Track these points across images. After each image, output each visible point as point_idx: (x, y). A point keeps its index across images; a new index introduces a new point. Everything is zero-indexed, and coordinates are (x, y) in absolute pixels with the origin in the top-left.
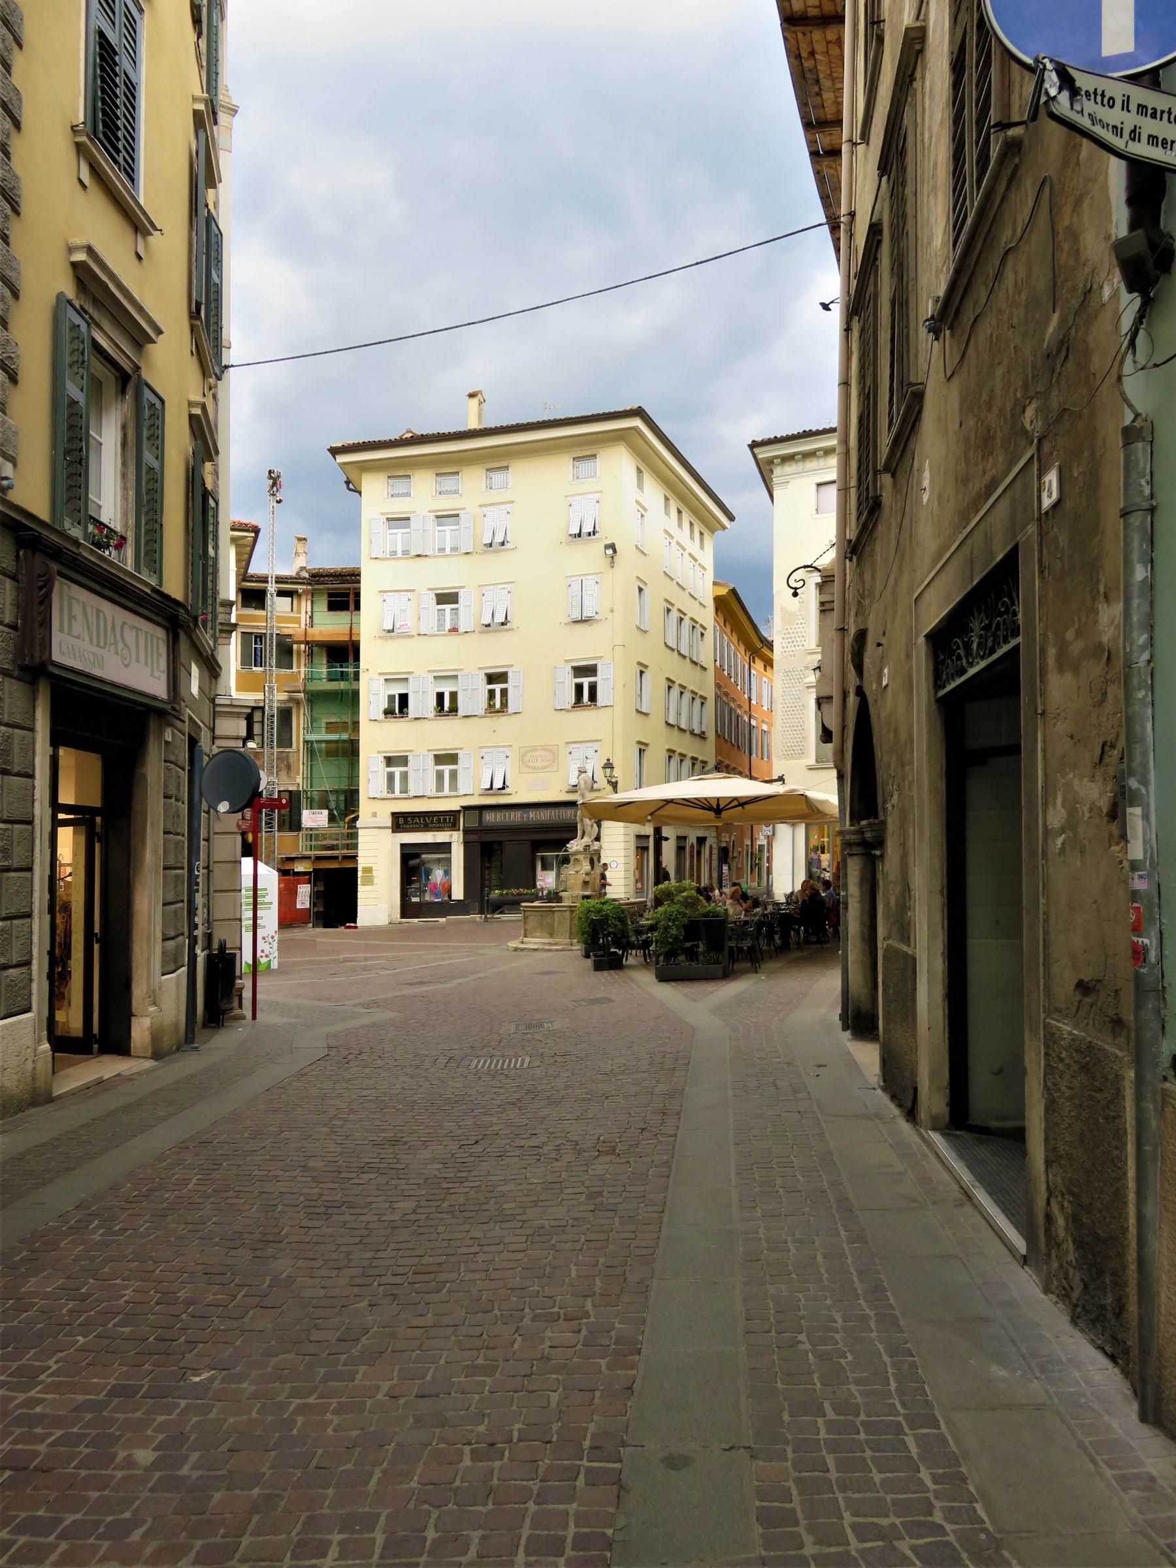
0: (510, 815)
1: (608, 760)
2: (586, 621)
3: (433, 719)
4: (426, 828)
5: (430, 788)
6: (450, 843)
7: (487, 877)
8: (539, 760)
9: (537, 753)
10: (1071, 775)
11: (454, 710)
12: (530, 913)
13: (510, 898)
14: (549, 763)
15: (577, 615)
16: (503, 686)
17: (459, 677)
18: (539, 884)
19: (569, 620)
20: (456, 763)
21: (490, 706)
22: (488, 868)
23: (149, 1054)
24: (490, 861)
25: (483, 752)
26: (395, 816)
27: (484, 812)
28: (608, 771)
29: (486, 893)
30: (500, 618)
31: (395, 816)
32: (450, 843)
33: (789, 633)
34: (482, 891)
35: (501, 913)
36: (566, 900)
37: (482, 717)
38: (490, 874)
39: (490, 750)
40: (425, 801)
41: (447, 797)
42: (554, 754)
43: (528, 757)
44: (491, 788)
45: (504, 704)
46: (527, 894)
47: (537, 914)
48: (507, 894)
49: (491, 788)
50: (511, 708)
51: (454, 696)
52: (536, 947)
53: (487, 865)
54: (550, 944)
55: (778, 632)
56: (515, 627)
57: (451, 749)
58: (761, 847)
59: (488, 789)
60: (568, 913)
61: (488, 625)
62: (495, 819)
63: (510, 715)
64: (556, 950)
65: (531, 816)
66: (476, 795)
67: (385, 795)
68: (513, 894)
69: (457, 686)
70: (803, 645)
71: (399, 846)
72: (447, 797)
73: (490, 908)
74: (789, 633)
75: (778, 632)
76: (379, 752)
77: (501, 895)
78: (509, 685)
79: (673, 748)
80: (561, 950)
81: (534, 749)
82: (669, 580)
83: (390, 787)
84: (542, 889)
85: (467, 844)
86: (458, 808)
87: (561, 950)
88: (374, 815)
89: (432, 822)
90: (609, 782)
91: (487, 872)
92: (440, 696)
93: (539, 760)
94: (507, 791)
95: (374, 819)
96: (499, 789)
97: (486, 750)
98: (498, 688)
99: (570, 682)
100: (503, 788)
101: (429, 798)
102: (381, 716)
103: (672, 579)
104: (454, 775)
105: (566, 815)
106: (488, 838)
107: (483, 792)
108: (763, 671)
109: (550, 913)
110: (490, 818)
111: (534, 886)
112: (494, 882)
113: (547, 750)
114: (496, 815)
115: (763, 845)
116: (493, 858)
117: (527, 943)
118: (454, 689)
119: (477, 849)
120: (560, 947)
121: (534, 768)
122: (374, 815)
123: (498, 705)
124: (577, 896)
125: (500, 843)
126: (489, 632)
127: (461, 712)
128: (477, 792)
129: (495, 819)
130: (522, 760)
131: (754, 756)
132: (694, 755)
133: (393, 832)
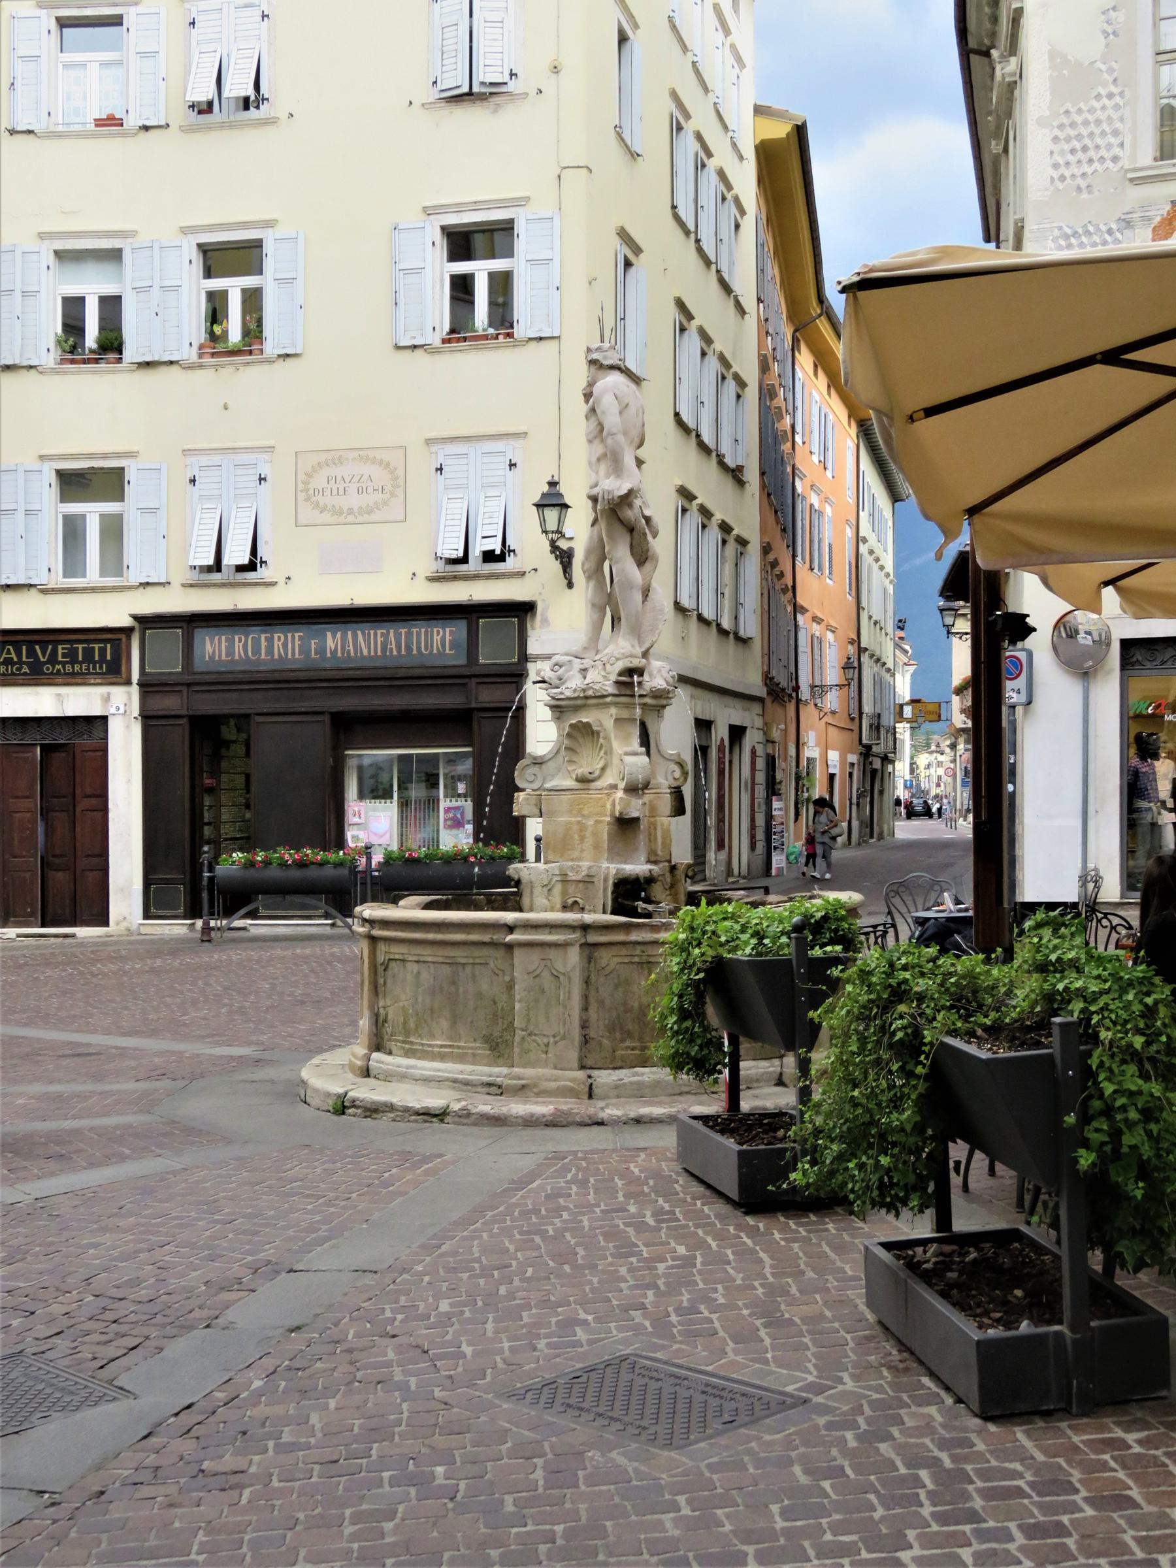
0: (270, 641)
1: (553, 484)
2: (483, 97)
3: (54, 371)
4: (36, 676)
6: (104, 719)
7: (207, 816)
8: (352, 489)
11: (111, 345)
12: (397, 951)
13: (274, 873)
14: (378, 497)
15: (457, 80)
16: (250, 281)
17: (127, 256)
18: (354, 837)
19: (434, 94)
20: (120, 497)
21: (213, 337)
22: (211, 790)
23: (476, 715)
24: (215, 773)
25: (193, 466)
28: (551, 515)
29: (205, 858)
30: (239, 85)
32: (104, 719)
33: (1073, 125)
34: (195, 853)
35: (253, 915)
36: (540, 900)
37: (190, 367)
38: (216, 807)
39: (216, 459)
41: (94, 590)
42: (392, 472)
43: (319, 482)
44: (217, 566)
45: (254, 333)
46: (321, 864)
47: (427, 953)
48: (267, 863)
49: (217, 566)
50: (273, 342)
51: (111, 306)
52: (434, 1100)
53: (208, 781)
54: (495, 1089)
55: (1041, 122)
56: (283, 115)
57: (105, 456)
58: (811, 761)
59: (209, 569)
60: (574, 956)
61: (206, 108)
62: (230, 652)
63: (269, 361)
64: (530, 1122)
65: (330, 644)
68: (283, 865)
69: (120, 279)
70: (1115, 159)
72: (94, 590)
73: (219, 903)
74: (1073, 125)
75: (1041, 122)
77: (251, 864)
78: (267, 281)
79: (693, 488)
80: (552, 1123)
81: (337, 458)
82: (677, 48)
84: (367, 850)
85: (149, 720)
86: (127, 622)
87: (552, 1123)
89: (53, 660)
90: (554, 547)
91: (207, 801)
92: (73, 307)
93: (352, 489)
94: (262, 573)
96: (240, 569)
97: (204, 460)
98: (234, 286)
100: (251, 567)
101: (45, 591)
103: (685, 49)
104: (113, 530)
106: (208, 705)
107: (194, 577)
108: (811, 373)
109: (496, 958)
111: (340, 843)
112: (227, 830)
113: (374, 461)
114: (231, 642)
115: (813, 760)
116: (224, 764)
117: (388, 1077)
118: (110, 289)
119: (178, 738)
120: (542, 1108)
123: (235, 335)
124: (588, 881)
125: (243, 720)
126: (209, 128)
127: (131, 353)
128: (178, 578)
129: (230, 652)
130: (305, 491)
131: (799, 558)
132: (728, 520)
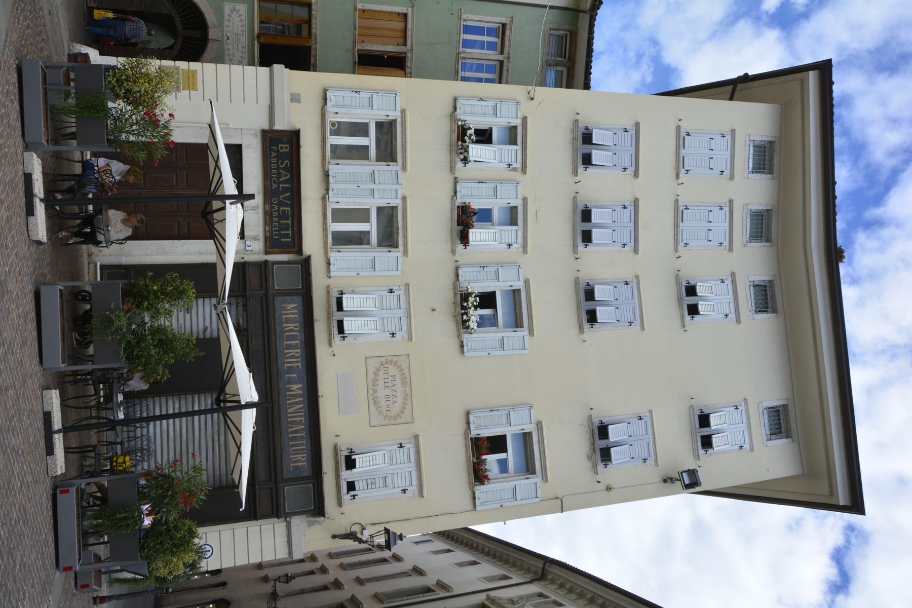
0: (295, 347)
5: (341, 200)
8: (388, 392)
9: (399, 388)
10: (105, 521)
14: (384, 408)
26: (294, 137)
27: (299, 299)
31: (294, 137)
40: (320, 192)
42: (399, 416)
43: (392, 370)
56: (584, 336)
57: (405, 237)
62: (288, 321)
66: (329, 281)
67: (330, 118)
71: (240, 143)
76: (403, 112)
83: (340, 129)
88: (295, 98)
89: (280, 204)
93: (388, 392)
95: (287, 98)
99: (500, 287)
102: (459, 201)
105: (297, 452)
110: (290, 310)
113: (405, 403)
121: (375, 383)
122: (295, 98)
129: (288, 321)
130: (388, 361)
133: (264, 132)
